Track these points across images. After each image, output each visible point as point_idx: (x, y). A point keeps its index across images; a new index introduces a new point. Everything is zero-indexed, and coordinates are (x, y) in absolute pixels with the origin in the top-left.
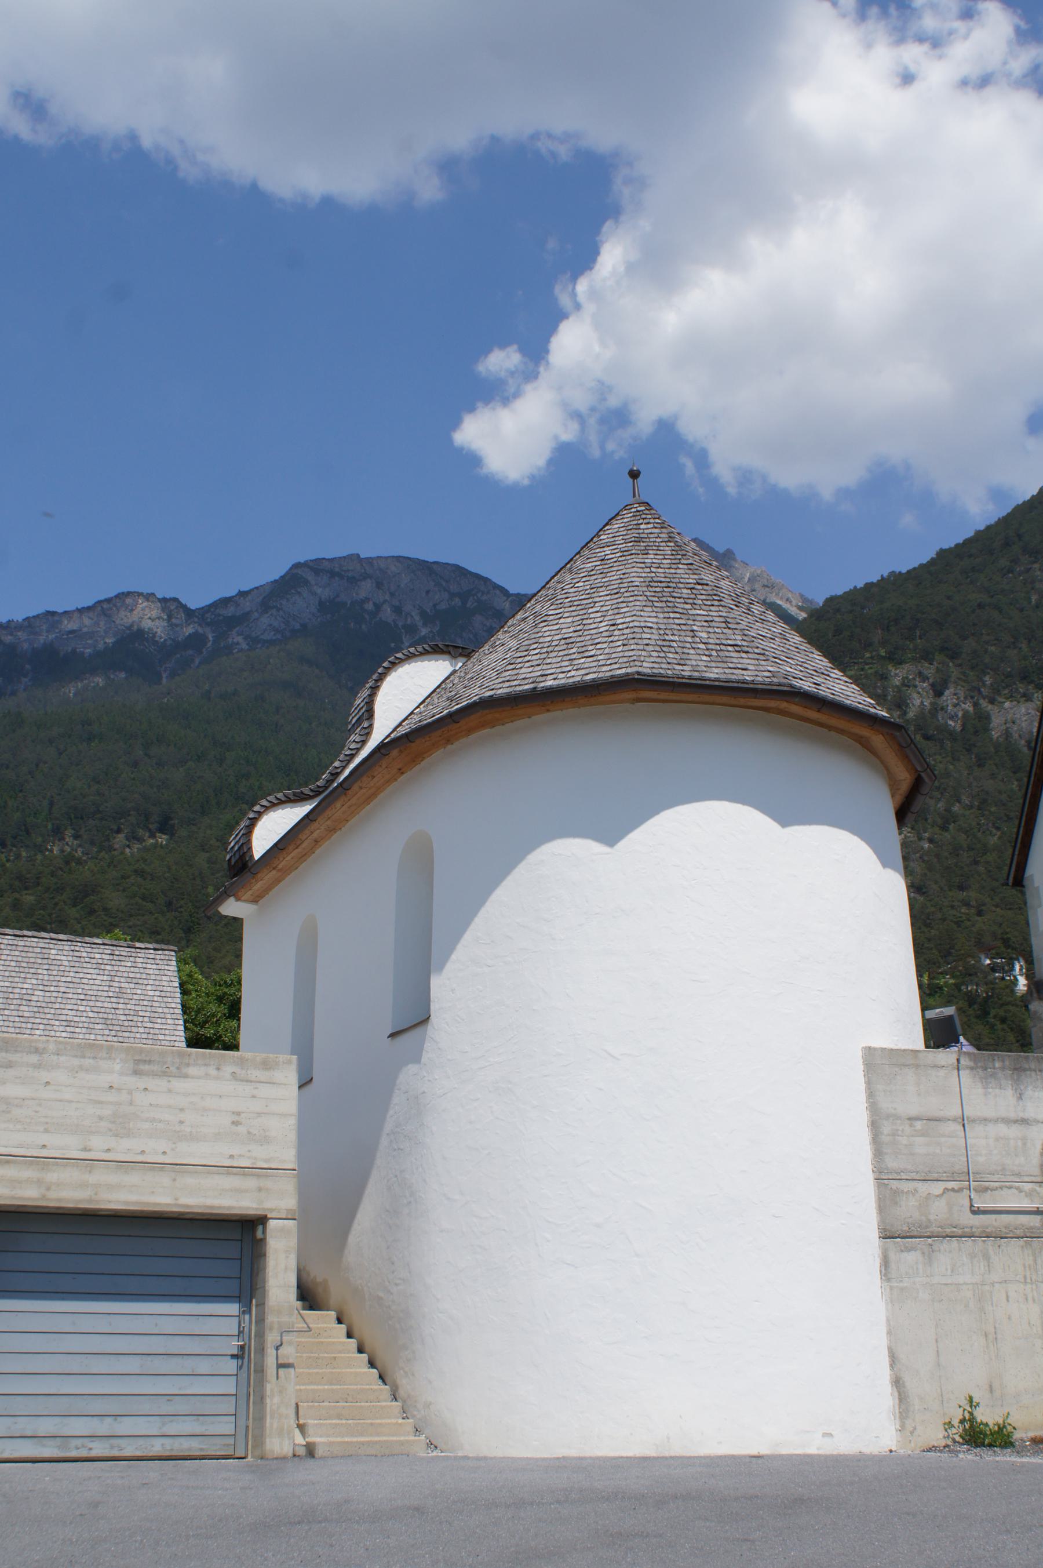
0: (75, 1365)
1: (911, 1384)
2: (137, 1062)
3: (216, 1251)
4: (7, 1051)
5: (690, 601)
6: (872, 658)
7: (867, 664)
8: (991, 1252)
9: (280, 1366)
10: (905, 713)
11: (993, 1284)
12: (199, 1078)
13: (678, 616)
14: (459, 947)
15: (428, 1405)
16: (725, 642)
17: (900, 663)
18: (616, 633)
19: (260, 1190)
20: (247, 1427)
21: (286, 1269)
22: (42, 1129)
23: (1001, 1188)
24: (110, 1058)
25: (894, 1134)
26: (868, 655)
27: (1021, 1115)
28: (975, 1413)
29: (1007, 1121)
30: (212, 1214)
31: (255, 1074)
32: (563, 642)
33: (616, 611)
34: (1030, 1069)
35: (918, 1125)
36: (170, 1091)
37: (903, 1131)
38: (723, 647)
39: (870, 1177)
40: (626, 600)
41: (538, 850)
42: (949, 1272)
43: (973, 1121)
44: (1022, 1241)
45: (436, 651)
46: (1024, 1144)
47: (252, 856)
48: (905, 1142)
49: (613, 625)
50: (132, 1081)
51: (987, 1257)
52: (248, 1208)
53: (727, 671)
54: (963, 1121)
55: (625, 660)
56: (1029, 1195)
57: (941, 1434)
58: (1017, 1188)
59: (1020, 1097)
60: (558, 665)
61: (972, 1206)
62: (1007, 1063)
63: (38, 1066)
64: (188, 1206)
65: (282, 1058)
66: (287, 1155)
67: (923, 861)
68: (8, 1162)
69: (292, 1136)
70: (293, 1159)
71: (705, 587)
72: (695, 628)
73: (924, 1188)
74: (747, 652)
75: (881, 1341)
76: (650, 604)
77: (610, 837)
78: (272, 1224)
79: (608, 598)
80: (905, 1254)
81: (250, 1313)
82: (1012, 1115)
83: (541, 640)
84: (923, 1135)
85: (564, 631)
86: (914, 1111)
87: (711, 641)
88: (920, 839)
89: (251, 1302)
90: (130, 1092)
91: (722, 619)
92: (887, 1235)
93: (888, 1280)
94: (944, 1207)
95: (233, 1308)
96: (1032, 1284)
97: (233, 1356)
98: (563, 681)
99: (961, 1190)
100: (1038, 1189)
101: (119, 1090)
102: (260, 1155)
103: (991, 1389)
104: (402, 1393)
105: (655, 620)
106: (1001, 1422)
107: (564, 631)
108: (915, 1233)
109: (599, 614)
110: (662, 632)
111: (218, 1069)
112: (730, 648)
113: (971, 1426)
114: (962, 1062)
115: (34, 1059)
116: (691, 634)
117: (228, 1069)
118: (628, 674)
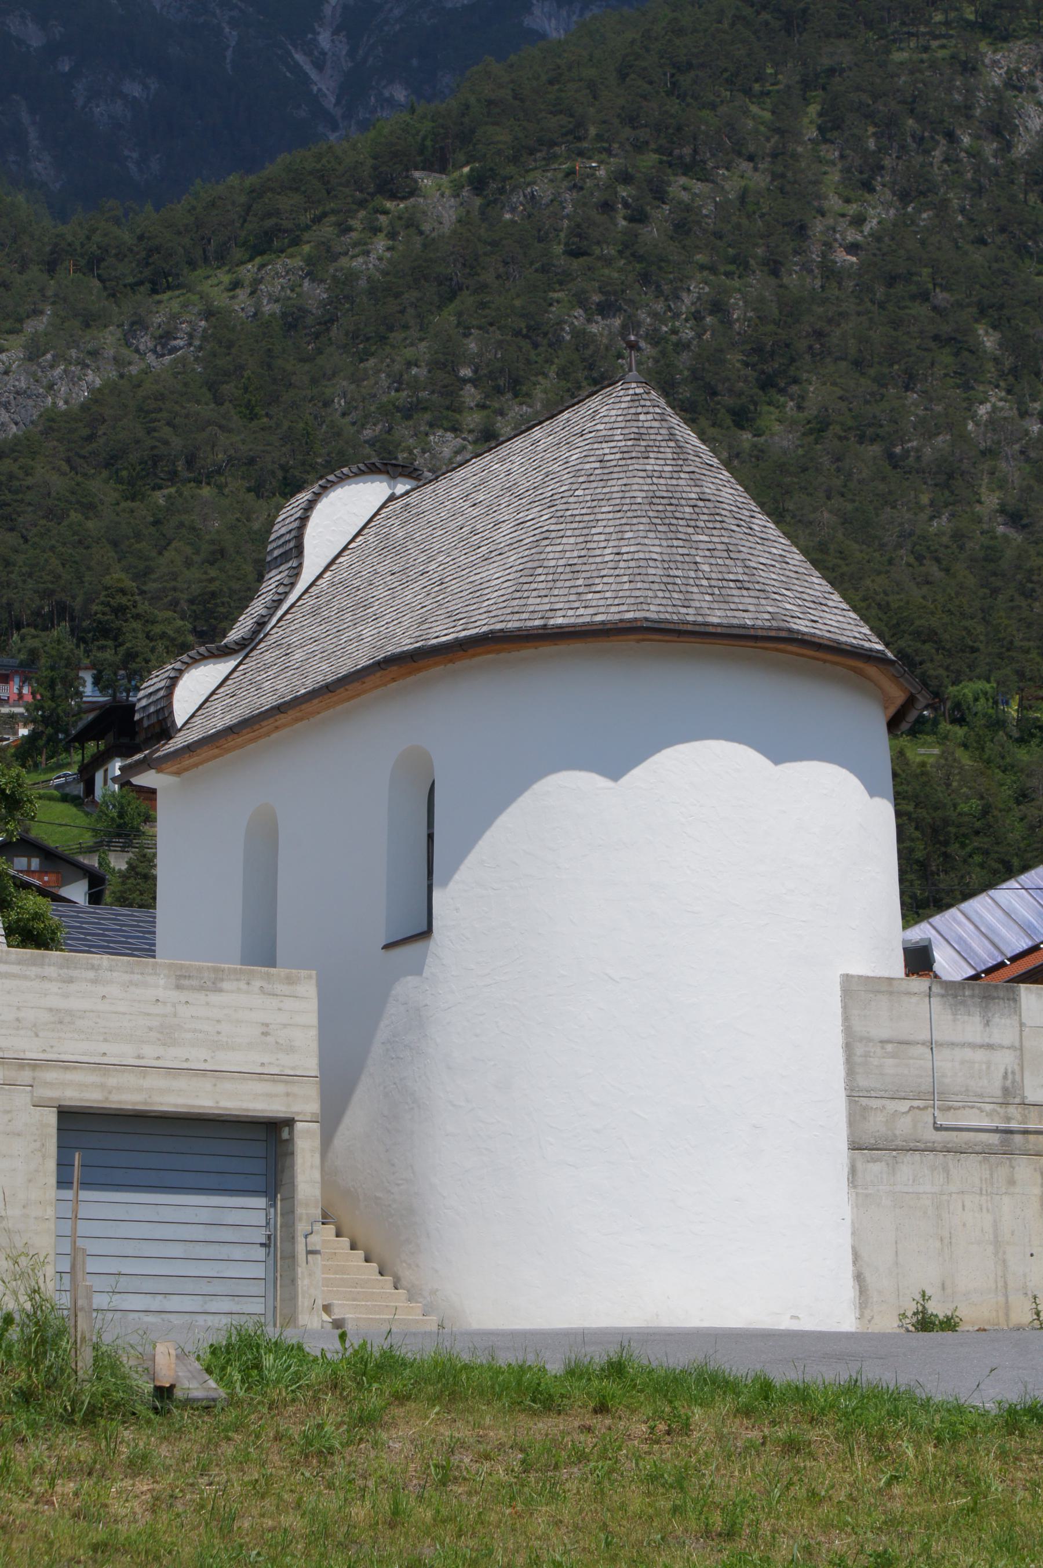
0: (129, 1248)
1: (870, 1279)
2: (179, 977)
3: (248, 1151)
4: (68, 968)
5: (692, 523)
6: (947, 23)
7: (936, 37)
8: (951, 1166)
9: (309, 1252)
10: (1009, 146)
11: (950, 1194)
12: (232, 992)
13: (681, 543)
14: (463, 867)
15: (434, 1292)
16: (727, 577)
17: (1005, 39)
18: (622, 564)
19: (288, 1095)
20: (275, 1307)
21: (312, 1167)
22: (101, 1039)
23: (964, 1107)
24: (155, 974)
25: (866, 1055)
26: (939, 17)
27: (987, 1040)
28: (927, 1306)
29: (973, 1046)
30: (247, 1116)
31: (280, 988)
32: (568, 569)
33: (620, 536)
34: (998, 998)
35: (889, 1047)
36: (207, 1004)
37: (874, 1052)
38: (725, 583)
39: (843, 1094)
40: (630, 521)
41: (544, 781)
42: (911, 1182)
43: (941, 1045)
44: (980, 1157)
45: (372, 470)
46: (988, 1068)
47: (174, 721)
48: (876, 1063)
49: (618, 554)
50: (174, 995)
51: (946, 1170)
52: (278, 1111)
53: (729, 613)
54: (931, 1045)
55: (632, 600)
56: (989, 1115)
57: (896, 1323)
58: (979, 1108)
59: (987, 1024)
60: (566, 599)
61: (935, 1123)
62: (977, 992)
63: (95, 982)
64: (226, 1109)
65: (303, 973)
66: (310, 1065)
67: (1028, 460)
68: (75, 1068)
69: (314, 1046)
70: (316, 1067)
71: (708, 504)
72: (698, 559)
73: (892, 1106)
74: (748, 589)
75: (846, 1241)
76: (653, 528)
77: (615, 771)
78: (299, 1126)
79: (611, 516)
80: (871, 1165)
81: (275, 1205)
82: (978, 1040)
83: (546, 563)
84: (892, 1057)
85: (568, 555)
86: (885, 1033)
87: (714, 576)
88: (1024, 414)
89: (276, 1196)
90: (174, 1005)
91: (724, 547)
92: (855, 1146)
93: (855, 1187)
94: (907, 1122)
95: (261, 1202)
96: (987, 1195)
97: (262, 1245)
98: (572, 620)
99: (926, 1108)
100: (999, 1109)
101: (165, 1003)
102: (286, 1063)
103: (943, 1288)
104: (404, 1282)
105: (658, 549)
106: (949, 1314)
107: (568, 555)
108: (881, 1146)
109: (603, 537)
110: (666, 566)
111: (248, 984)
112: (732, 584)
113: (923, 1318)
114: (934, 989)
115: (91, 974)
116: (693, 567)
117: (257, 984)
118: (636, 620)
